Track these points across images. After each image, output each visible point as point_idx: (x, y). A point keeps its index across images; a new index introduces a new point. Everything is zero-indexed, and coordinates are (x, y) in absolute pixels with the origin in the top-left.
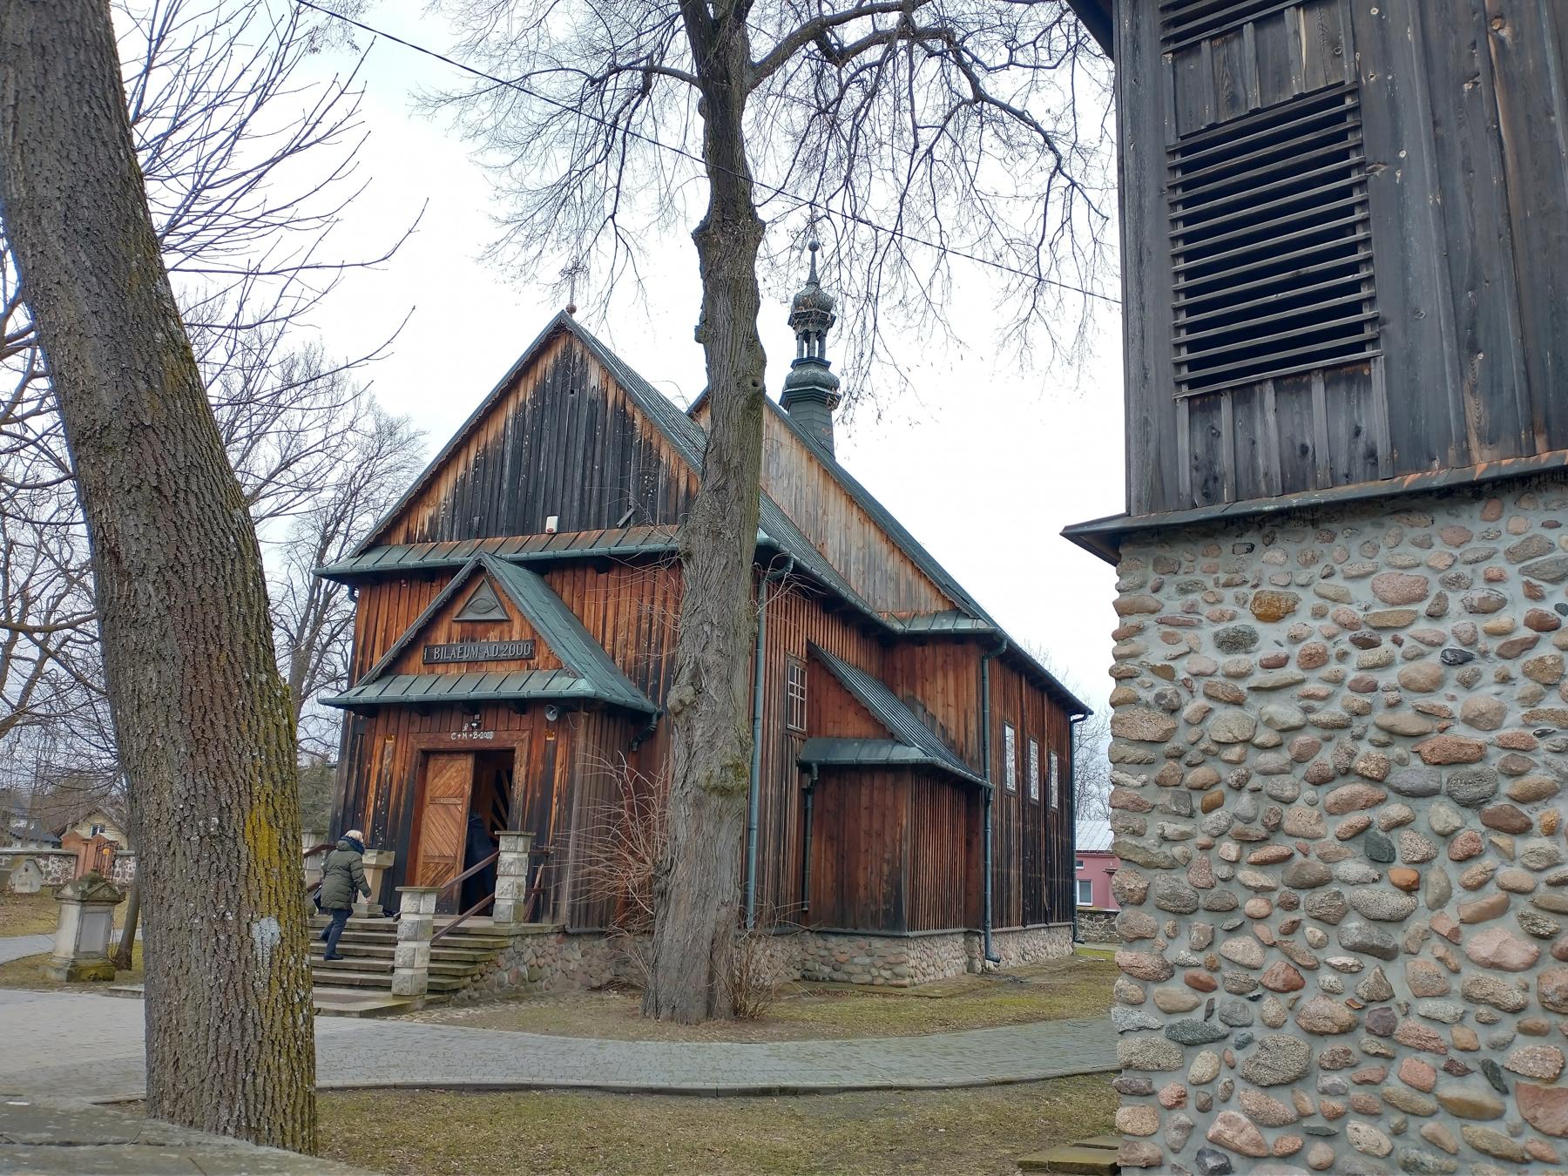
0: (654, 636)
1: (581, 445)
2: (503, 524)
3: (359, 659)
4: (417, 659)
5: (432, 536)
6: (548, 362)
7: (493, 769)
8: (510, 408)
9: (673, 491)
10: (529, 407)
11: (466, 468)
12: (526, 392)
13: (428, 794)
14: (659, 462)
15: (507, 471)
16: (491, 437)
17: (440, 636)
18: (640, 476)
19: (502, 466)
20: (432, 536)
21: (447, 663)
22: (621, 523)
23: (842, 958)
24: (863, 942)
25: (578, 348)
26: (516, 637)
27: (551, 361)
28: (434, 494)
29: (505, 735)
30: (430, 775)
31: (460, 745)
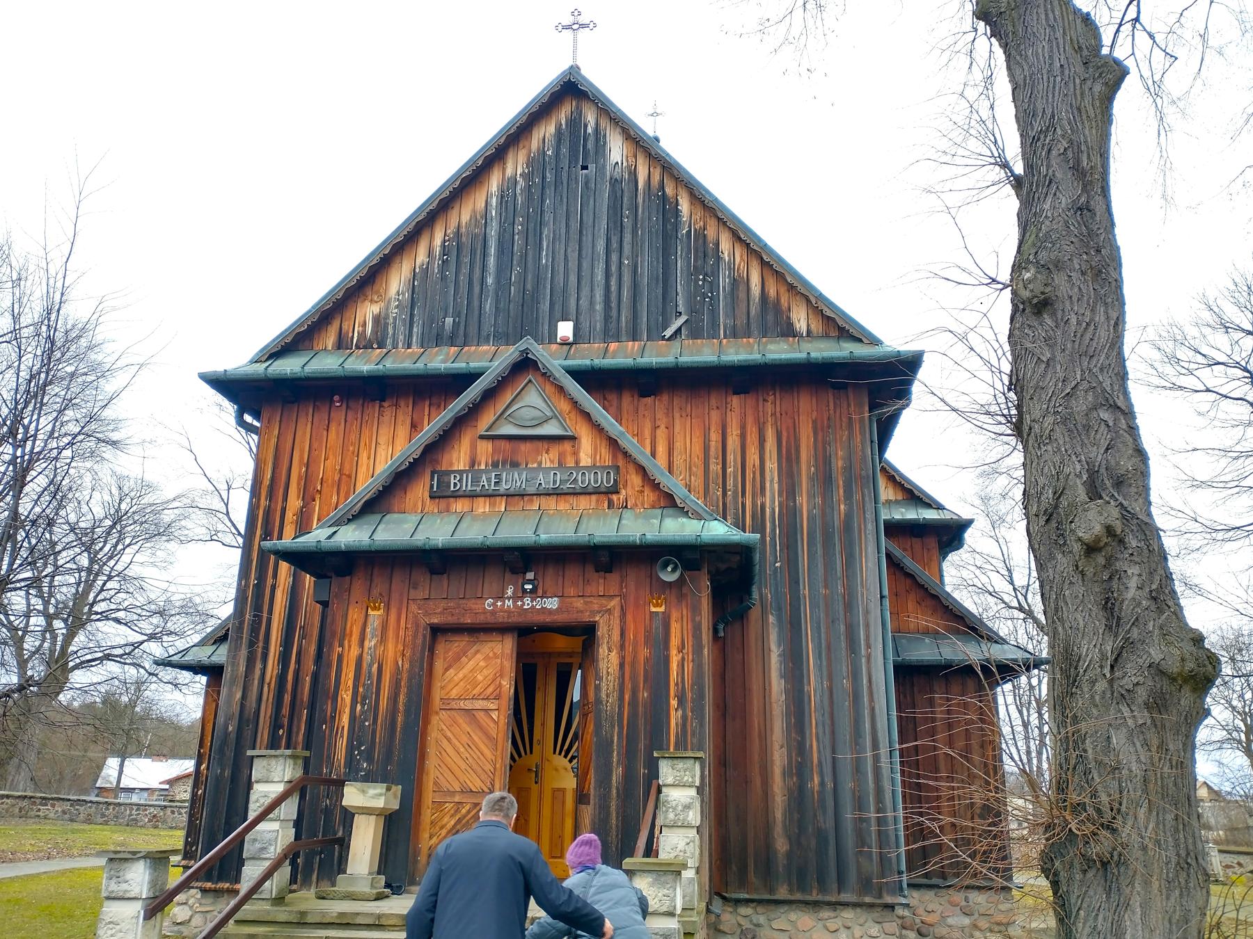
0: (730, 482)
1: (603, 232)
2: (488, 327)
3: (264, 503)
4: (420, 490)
5: (378, 340)
6: (547, 131)
7: (547, 662)
8: (494, 183)
9: (742, 295)
10: (521, 182)
11: (430, 253)
12: (516, 165)
13: (437, 694)
14: (718, 259)
15: (492, 261)
16: (465, 217)
17: (457, 458)
18: (692, 274)
19: (485, 255)
20: (378, 340)
21: (472, 496)
22: (668, 333)
23: (929, 919)
24: (959, 897)
25: (590, 117)
26: (585, 460)
27: (551, 129)
28: (379, 285)
29: (579, 604)
30: (439, 665)
31: (501, 618)
